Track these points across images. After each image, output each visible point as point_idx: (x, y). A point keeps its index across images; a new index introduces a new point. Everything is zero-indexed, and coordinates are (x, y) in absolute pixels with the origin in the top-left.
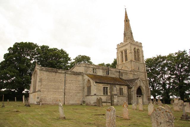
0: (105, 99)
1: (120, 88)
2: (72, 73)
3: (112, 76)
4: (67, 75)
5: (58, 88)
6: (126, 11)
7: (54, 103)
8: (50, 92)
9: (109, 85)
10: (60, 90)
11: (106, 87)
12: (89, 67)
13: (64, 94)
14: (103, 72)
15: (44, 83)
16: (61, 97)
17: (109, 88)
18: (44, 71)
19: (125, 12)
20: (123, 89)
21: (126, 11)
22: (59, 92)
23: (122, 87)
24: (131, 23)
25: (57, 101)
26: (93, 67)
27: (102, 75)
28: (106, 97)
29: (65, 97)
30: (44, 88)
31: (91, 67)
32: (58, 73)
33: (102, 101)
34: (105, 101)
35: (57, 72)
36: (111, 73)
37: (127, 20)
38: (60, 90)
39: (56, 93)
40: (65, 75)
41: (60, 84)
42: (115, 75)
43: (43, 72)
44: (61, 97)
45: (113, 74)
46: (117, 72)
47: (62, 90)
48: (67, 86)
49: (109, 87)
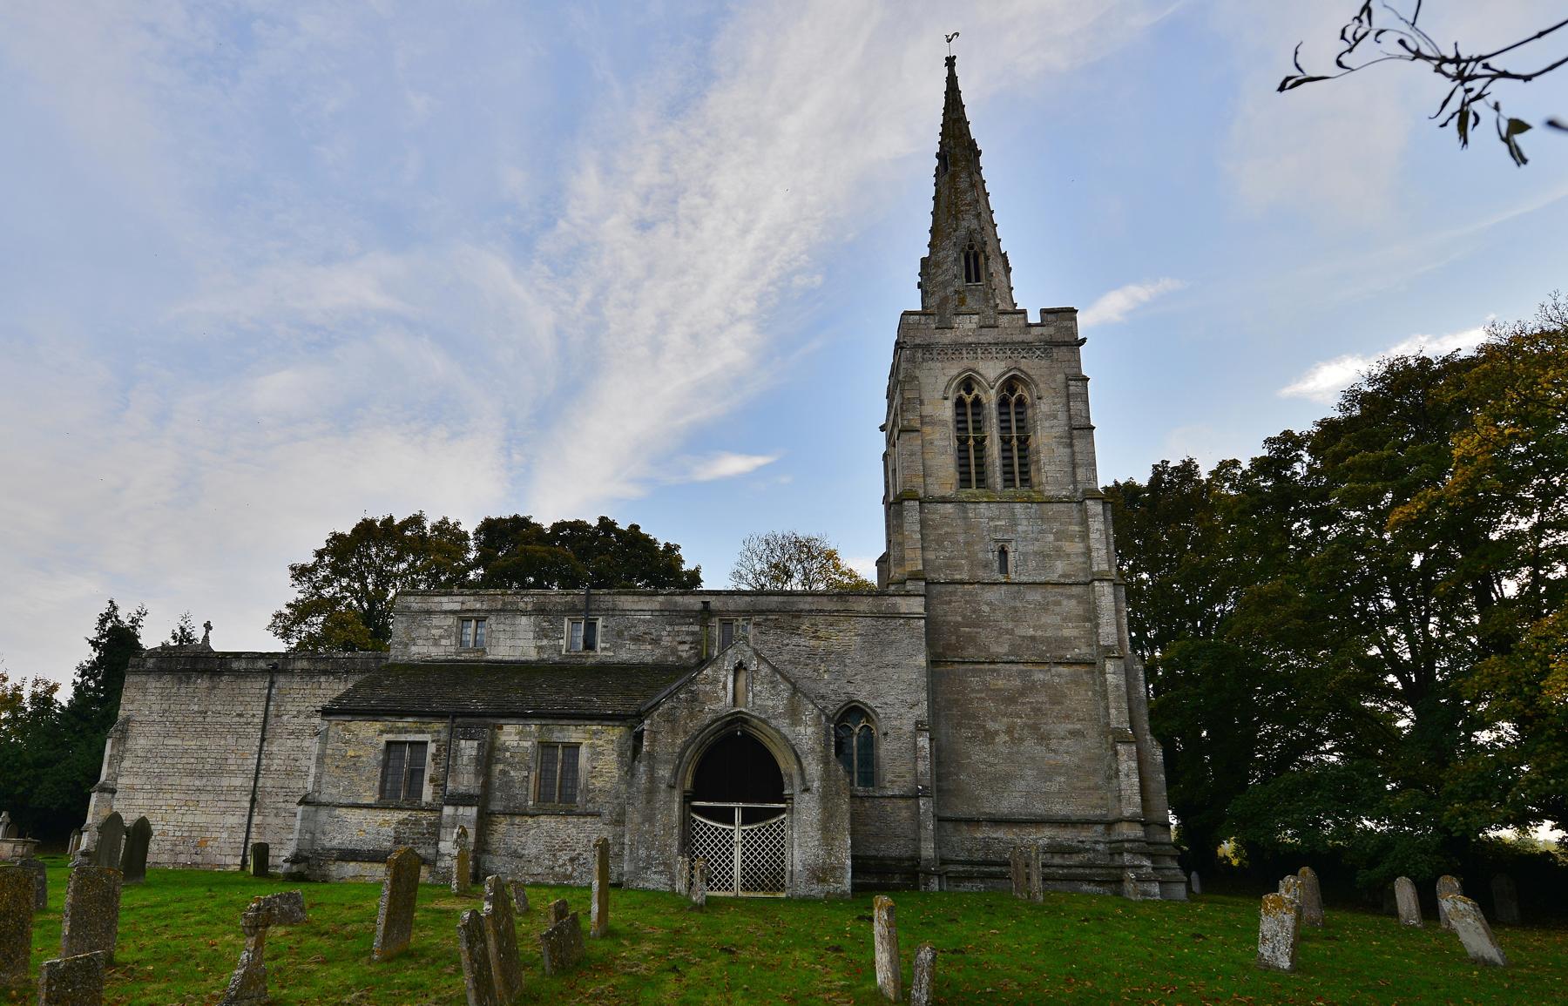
0: (389, 831)
1: (547, 747)
2: (321, 666)
3: (624, 655)
4: (281, 681)
5: (220, 770)
6: (952, 80)
7: (182, 859)
8: (168, 796)
10: (225, 782)
11: (412, 743)
12: (429, 612)
13: (248, 805)
15: (142, 741)
17: (432, 748)
18: (148, 672)
21: (952, 80)
22: (217, 791)
23: (573, 734)
24: (990, 168)
26: (457, 607)
27: (533, 655)
28: (403, 815)
29: (256, 819)
31: (447, 607)
33: (1087, 874)
35: (220, 674)
36: (620, 635)
38: (225, 782)
39: (203, 797)
40: (272, 683)
41: (231, 740)
42: (656, 642)
43: (144, 678)
45: (636, 639)
46: (687, 614)
47: (237, 782)
49: (430, 736)
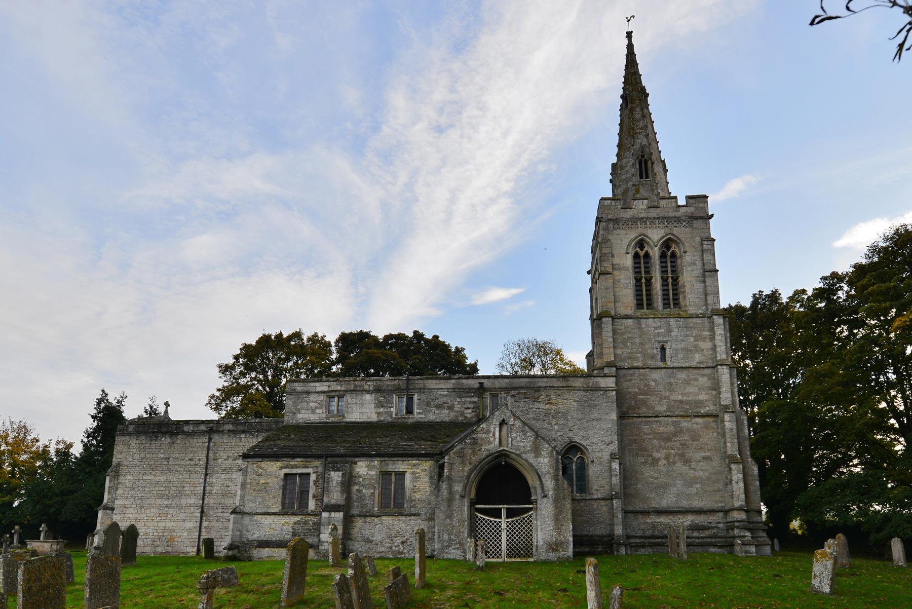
1: (385, 475)
2: (241, 428)
5: (180, 494)
6: (630, 47)
7: (159, 549)
8: (148, 511)
9: (317, 463)
10: (184, 501)
11: (300, 474)
13: (199, 515)
14: (379, 404)
15: (129, 477)
16: (189, 525)
17: (313, 477)
18: (130, 434)
19: (625, 51)
20: (408, 477)
21: (630, 47)
23: (401, 466)
25: (169, 540)
26: (326, 389)
27: (374, 418)
29: (205, 524)
30: (127, 498)
31: (319, 389)
32: (180, 437)
34: (358, 546)
36: (428, 404)
37: (634, 95)
39: (170, 511)
40: (210, 439)
41: (186, 475)
42: (451, 408)
43: (127, 438)
44: (189, 525)
45: (439, 407)
47: (192, 501)
48: (214, 480)
49: (312, 469)
